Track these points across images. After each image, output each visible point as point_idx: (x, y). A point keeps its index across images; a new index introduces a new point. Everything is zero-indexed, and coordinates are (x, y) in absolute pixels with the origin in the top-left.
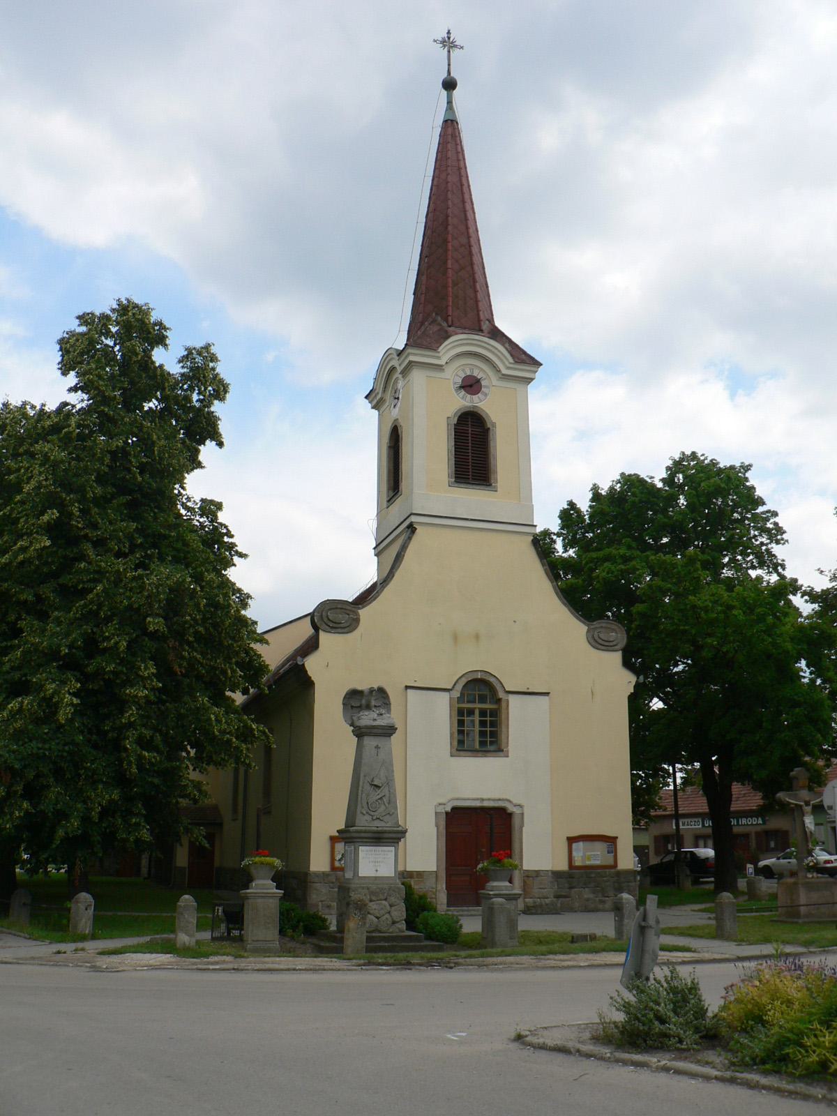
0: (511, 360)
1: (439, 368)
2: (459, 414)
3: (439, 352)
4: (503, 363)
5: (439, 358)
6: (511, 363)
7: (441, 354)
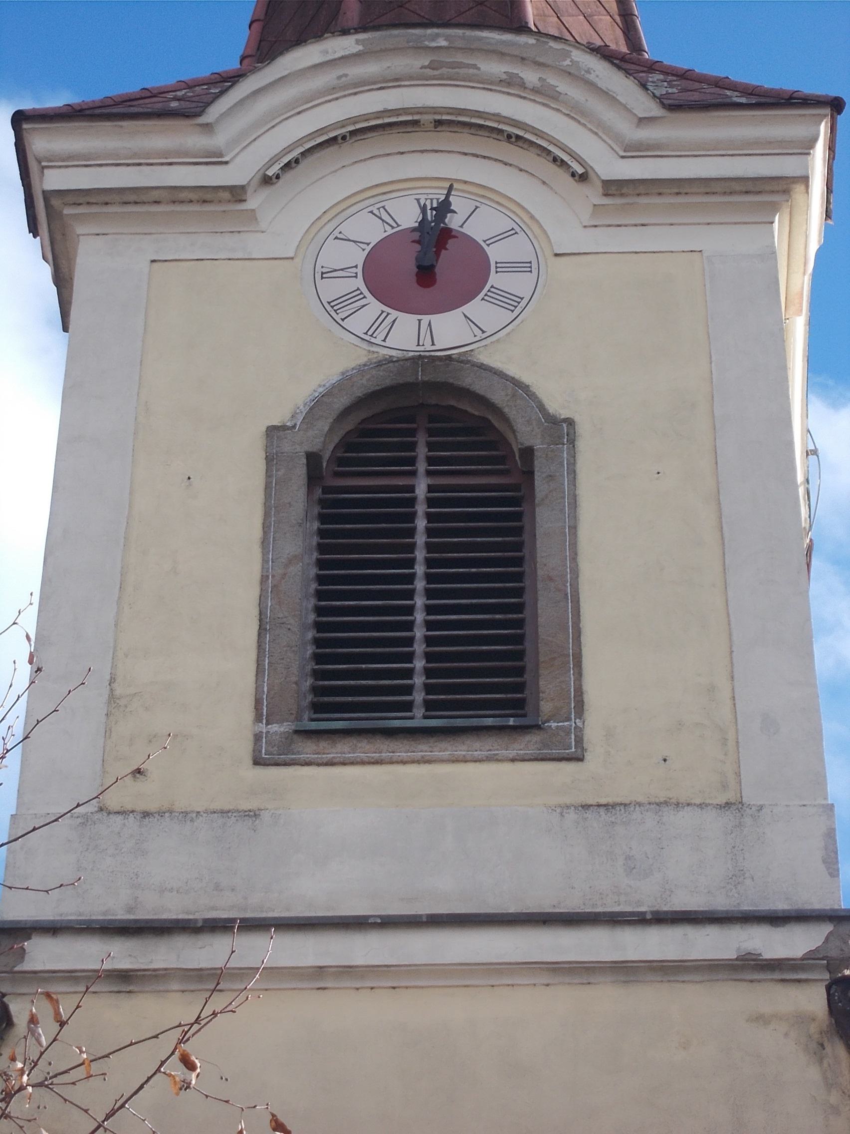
0: (645, 105)
1: (226, 163)
2: (342, 402)
3: (208, 128)
4: (600, 129)
5: (215, 159)
6: (642, 121)
7: (219, 140)
